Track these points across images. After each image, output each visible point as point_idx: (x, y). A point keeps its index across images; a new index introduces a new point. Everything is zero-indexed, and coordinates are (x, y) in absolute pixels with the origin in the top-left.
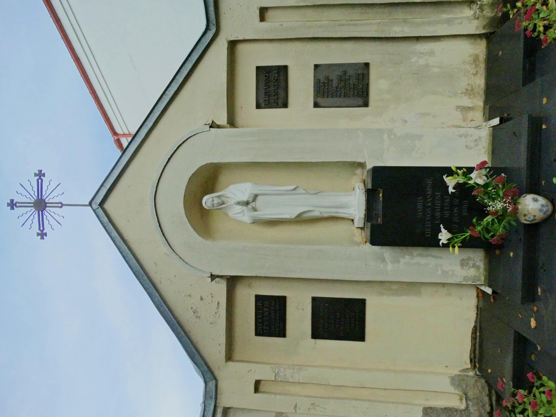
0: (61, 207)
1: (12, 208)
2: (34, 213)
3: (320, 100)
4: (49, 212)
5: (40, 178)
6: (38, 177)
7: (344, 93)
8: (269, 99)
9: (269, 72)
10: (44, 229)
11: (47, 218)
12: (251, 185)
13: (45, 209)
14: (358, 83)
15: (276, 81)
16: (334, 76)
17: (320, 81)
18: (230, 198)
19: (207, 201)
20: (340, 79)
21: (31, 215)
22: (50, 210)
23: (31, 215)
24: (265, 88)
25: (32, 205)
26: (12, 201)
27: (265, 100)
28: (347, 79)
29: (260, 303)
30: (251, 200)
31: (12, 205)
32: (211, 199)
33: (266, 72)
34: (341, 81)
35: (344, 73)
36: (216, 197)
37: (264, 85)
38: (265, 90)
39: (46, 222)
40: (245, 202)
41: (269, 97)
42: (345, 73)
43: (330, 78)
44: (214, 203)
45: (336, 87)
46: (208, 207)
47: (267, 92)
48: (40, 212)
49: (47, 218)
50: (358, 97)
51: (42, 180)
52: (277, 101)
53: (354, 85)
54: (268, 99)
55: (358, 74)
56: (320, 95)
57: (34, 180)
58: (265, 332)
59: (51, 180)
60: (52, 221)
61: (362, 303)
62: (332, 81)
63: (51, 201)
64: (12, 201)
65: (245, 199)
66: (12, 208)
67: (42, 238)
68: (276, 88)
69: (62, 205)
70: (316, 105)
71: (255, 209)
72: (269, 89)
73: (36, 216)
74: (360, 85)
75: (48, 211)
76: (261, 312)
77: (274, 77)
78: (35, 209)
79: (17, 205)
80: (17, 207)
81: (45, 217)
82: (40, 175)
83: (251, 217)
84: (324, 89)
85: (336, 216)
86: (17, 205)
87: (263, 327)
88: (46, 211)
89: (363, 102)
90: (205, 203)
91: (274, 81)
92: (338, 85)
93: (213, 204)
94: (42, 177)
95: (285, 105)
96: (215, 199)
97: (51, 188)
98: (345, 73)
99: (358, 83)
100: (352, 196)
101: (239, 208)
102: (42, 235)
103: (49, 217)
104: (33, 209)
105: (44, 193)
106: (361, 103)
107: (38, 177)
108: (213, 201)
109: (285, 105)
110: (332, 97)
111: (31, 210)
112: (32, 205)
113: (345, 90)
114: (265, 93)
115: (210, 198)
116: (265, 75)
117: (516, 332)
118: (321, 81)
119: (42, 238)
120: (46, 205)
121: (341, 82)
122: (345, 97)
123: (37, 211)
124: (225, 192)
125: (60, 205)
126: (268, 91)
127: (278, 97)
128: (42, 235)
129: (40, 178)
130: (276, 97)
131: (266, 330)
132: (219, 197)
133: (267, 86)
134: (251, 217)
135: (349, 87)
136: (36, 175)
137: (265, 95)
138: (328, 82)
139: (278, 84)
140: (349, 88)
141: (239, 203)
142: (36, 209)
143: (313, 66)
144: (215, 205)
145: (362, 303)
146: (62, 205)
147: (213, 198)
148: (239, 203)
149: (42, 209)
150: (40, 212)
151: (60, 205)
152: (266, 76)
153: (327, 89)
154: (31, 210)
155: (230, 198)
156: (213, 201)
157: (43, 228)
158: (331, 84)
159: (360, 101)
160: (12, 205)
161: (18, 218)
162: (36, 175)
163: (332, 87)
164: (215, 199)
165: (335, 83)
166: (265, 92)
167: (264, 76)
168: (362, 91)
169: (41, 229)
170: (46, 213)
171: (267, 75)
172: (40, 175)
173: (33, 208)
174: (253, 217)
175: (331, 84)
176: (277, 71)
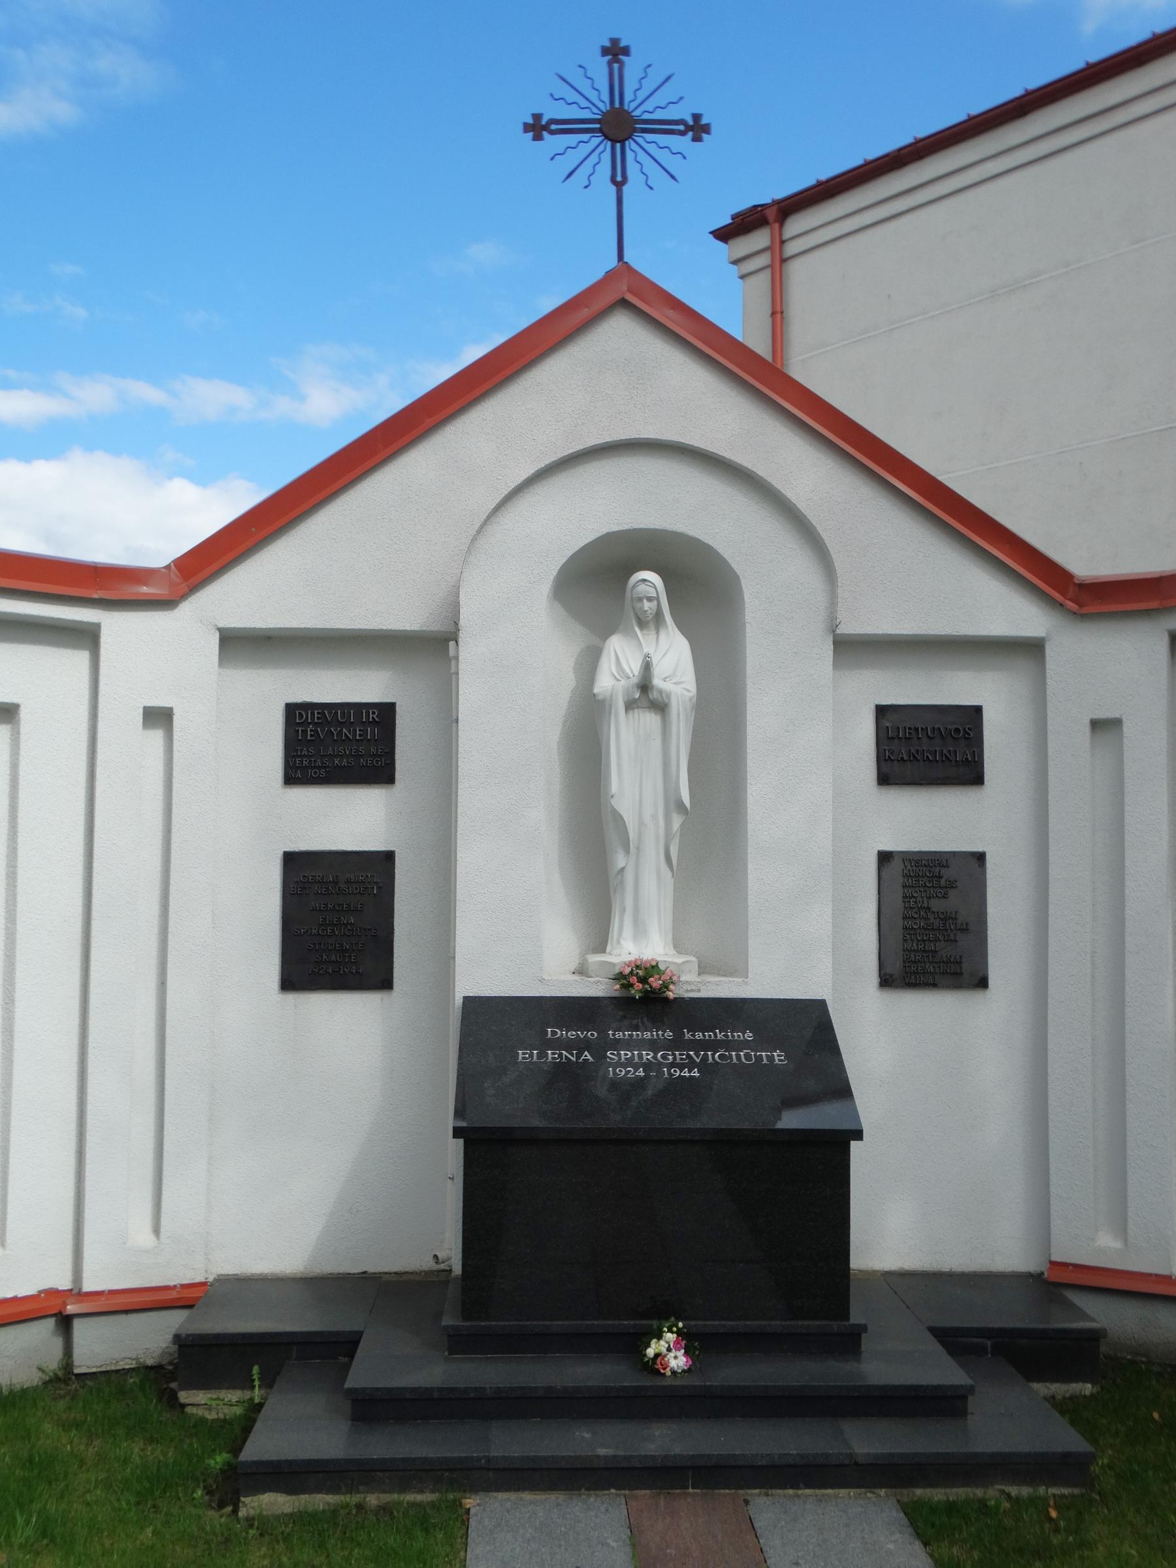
0: (613, 180)
1: (605, 51)
2: (595, 110)
3: (896, 866)
4: (598, 151)
5: (689, 128)
6: (691, 122)
7: (915, 927)
8: (901, 738)
9: (968, 738)
10: (552, 133)
11: (598, 163)
12: (692, 694)
13: (607, 137)
14: (940, 962)
15: (946, 756)
16: (954, 902)
17: (943, 866)
18: (657, 638)
19: (649, 581)
20: (948, 918)
21: (587, 99)
22: (603, 152)
23: (587, 99)
24: (927, 728)
25: (617, 105)
26: (626, 51)
27: (898, 728)
28: (948, 935)
29: (375, 716)
30: (654, 695)
31: (615, 52)
32: (655, 595)
33: (967, 730)
34: (945, 919)
35: (965, 927)
36: (659, 605)
37: (937, 726)
38: (922, 728)
39: (573, 139)
40: (650, 682)
41: (906, 738)
42: (965, 929)
43: (951, 892)
44: (645, 601)
45: (929, 908)
46: (634, 586)
47: (918, 734)
48: (598, 126)
49: (598, 163)
50: (904, 962)
51: (682, 133)
52: (894, 760)
53: (935, 952)
54: (901, 736)
55: (961, 962)
56: (909, 867)
57: (683, 112)
58: (298, 730)
59: (685, 158)
60: (573, 158)
61: (384, 983)
62: (945, 897)
63: (630, 156)
64: (626, 51)
65: (657, 682)
66: (605, 51)
67: (527, 128)
68: (927, 756)
69: (619, 185)
70: (884, 858)
71: (630, 705)
72: (925, 740)
73: (586, 115)
74: (934, 967)
75: (601, 148)
76: (352, 720)
77: (956, 751)
78: (608, 111)
79: (616, 66)
80: (610, 64)
81: (585, 137)
82: (697, 129)
83: (611, 696)
84: (923, 877)
85: (613, 909)
86: (616, 66)
87: (310, 723)
88: (602, 142)
89: (891, 976)
90: (644, 580)
91: (944, 752)
92: (933, 912)
93: (640, 600)
94: (690, 134)
95: (884, 779)
96: (654, 604)
97: (663, 156)
98: (965, 929)
99: (940, 962)
100: (665, 948)
101: (634, 667)
102: (537, 128)
103: (585, 149)
104: (630, 144)
105: (649, 137)
106: (888, 970)
107: (691, 122)
108: (650, 599)
109: (884, 779)
110: (905, 897)
111: (603, 102)
112: (617, 105)
113: (923, 931)
114: (917, 730)
115: (656, 588)
116: (959, 729)
117: (359, 1334)
118: (943, 871)
119: (527, 128)
120: (618, 142)
121: (942, 919)
122: (905, 928)
123: (599, 117)
124: (670, 628)
125: (619, 179)
126: (920, 736)
127: (905, 761)
128: (537, 128)
129: (689, 128)
130: (969, 757)
131: (305, 732)
132: (659, 615)
133: (934, 733)
134: (611, 696)
135: (929, 940)
136: (697, 117)
137: (910, 729)
138: (941, 888)
139: (937, 761)
140: (925, 939)
141: (647, 667)
142: (604, 114)
143: (979, 848)
144: (638, 605)
145: (384, 983)
146: (619, 185)
147: (658, 599)
148: (647, 667)
149: (605, 130)
150: (598, 126)
151: (619, 179)
152: (957, 730)
153: (925, 884)
154: (603, 102)
155: (657, 638)
156: (650, 599)
157: (553, 130)
158: (937, 896)
159: (896, 967)
160: (615, 52)
161: (580, 66)
162: (697, 117)
163: (930, 898)
164: (654, 604)
165: (936, 905)
166: (918, 728)
167: (956, 726)
168: (918, 973)
169: (553, 127)
170: (596, 141)
171: (961, 735)
172: (697, 129)
173: (608, 108)
174: (611, 700)
175: (937, 896)
176: (970, 759)
